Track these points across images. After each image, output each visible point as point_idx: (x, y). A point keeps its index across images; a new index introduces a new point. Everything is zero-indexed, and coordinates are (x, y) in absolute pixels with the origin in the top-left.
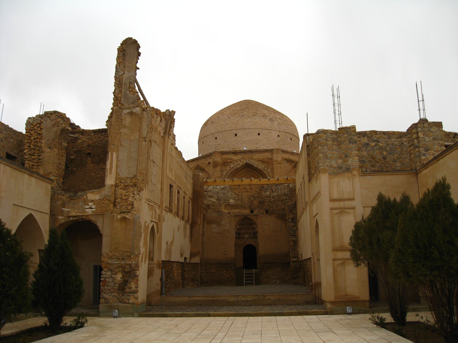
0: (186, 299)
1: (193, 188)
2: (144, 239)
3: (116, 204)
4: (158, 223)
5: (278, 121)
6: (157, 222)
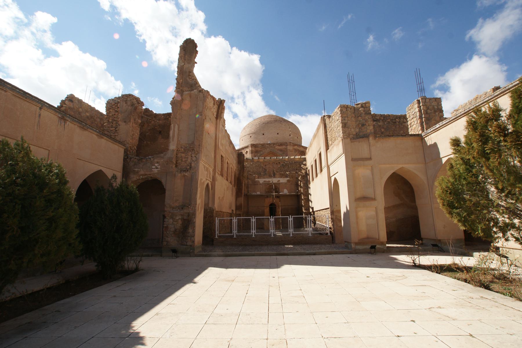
3: (177, 164)
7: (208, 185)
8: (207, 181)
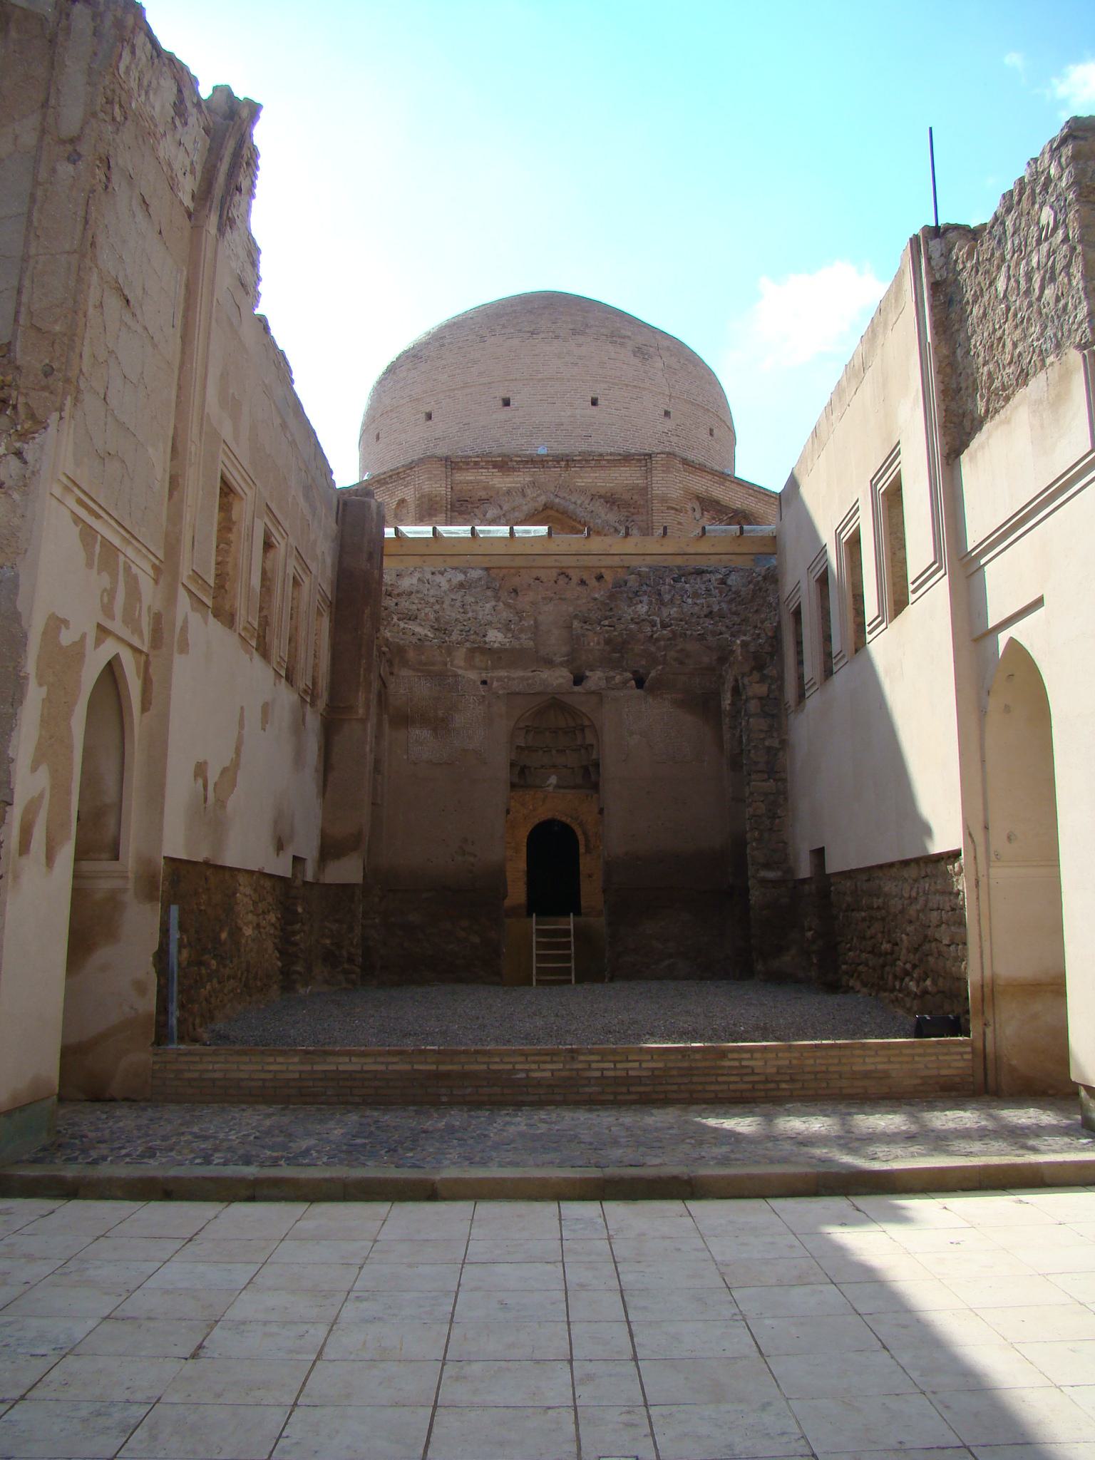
0: (288, 1066)
1: (340, 557)
2: (45, 722)
4: (147, 655)
5: (664, 359)
6: (145, 649)
7: (112, 671)
8: (109, 649)
